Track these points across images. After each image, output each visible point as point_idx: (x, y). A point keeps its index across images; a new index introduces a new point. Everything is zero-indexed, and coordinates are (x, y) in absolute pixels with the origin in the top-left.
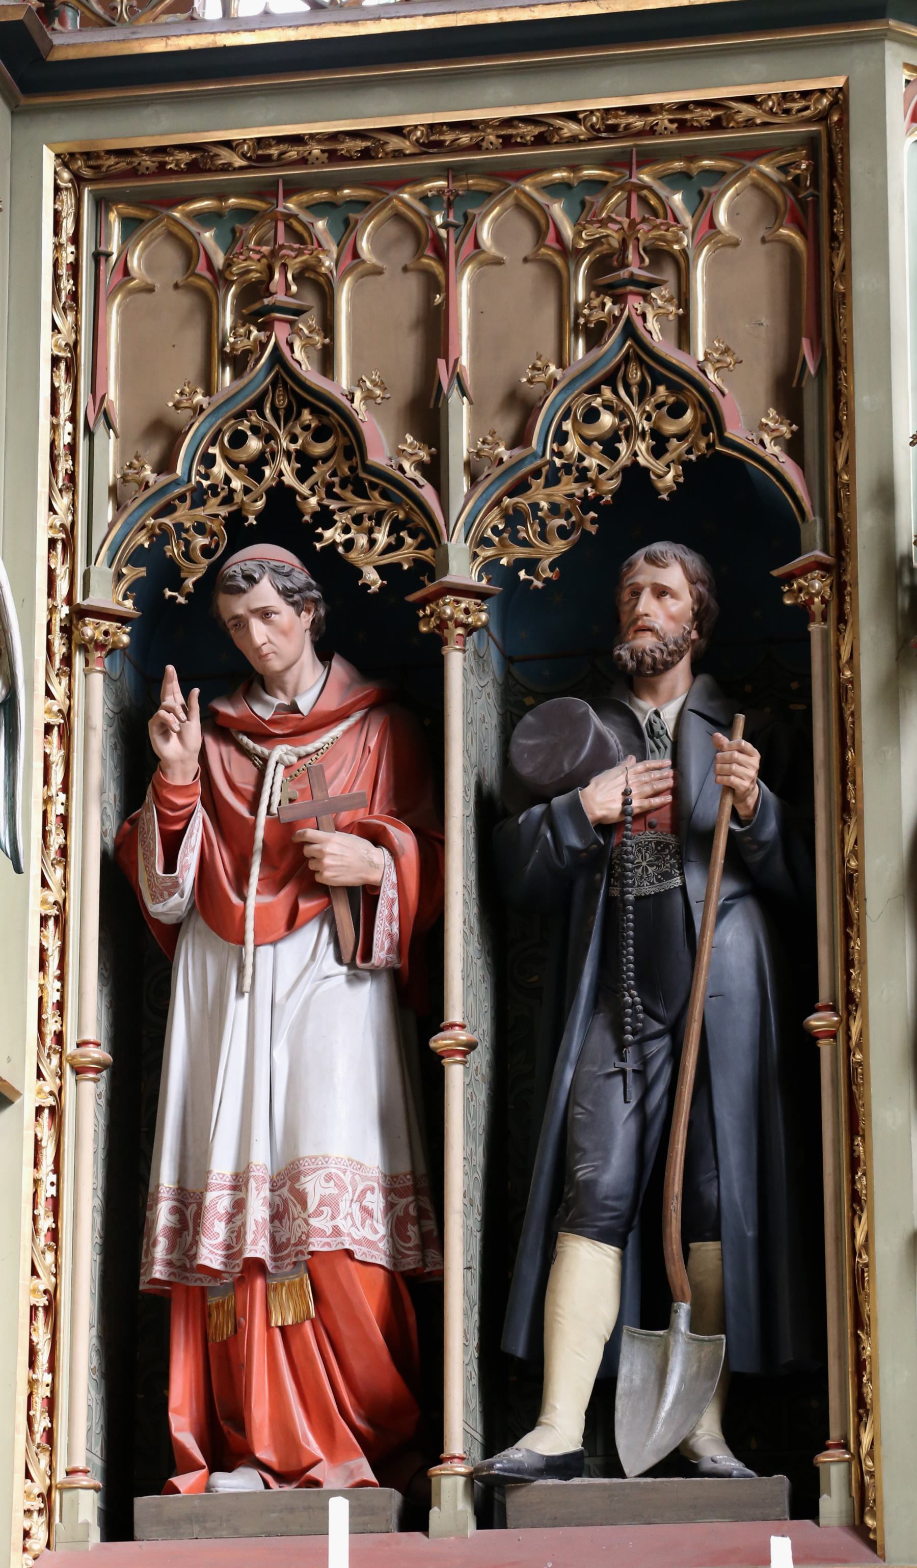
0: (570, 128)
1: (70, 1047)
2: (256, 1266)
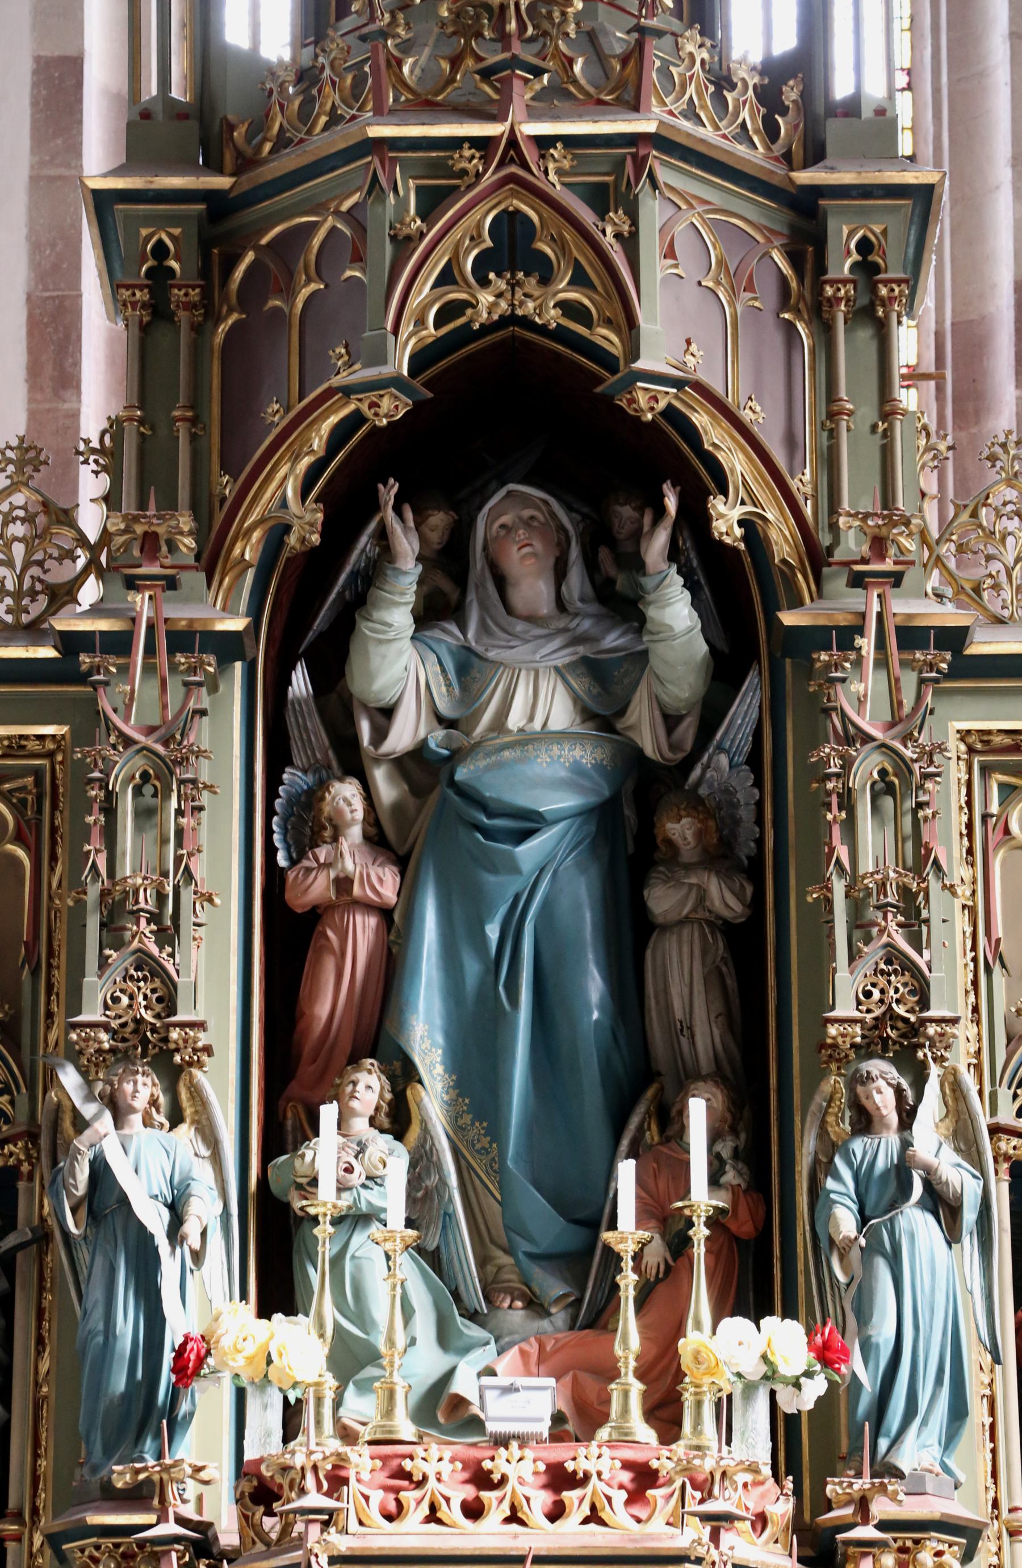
1: (1005, 1514)
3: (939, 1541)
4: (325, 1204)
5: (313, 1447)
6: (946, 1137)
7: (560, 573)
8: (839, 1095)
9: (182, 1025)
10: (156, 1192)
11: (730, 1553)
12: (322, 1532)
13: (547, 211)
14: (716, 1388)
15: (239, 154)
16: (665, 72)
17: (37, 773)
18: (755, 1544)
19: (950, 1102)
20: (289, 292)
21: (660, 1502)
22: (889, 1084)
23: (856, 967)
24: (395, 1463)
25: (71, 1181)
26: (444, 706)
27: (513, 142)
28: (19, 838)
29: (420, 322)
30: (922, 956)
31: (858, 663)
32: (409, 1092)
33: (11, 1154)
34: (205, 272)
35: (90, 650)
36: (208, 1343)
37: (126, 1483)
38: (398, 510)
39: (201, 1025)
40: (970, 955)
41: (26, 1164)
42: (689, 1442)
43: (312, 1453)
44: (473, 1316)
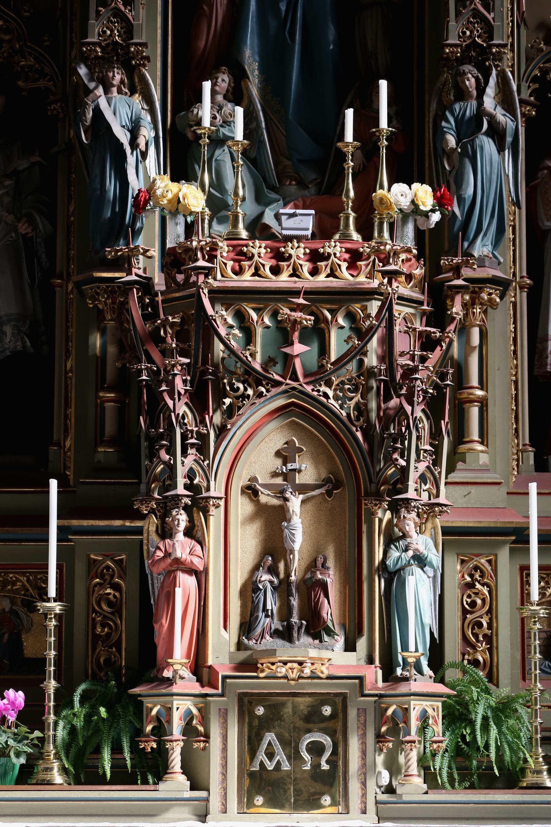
3: (491, 288)
4: (205, 128)
5: (201, 238)
6: (499, 103)
8: (448, 83)
9: (136, 44)
10: (124, 124)
11: (397, 289)
12: (205, 279)
14: (389, 216)
18: (407, 288)
19: (501, 86)
21: (363, 267)
22: (473, 76)
23: (458, 20)
24: (239, 248)
25: (84, 118)
30: (490, 14)
32: (242, 83)
33: (55, 109)
36: (150, 194)
37: (112, 256)
40: (510, 19)
41: (61, 114)
42: (377, 241)
43: (201, 241)
44: (273, 189)
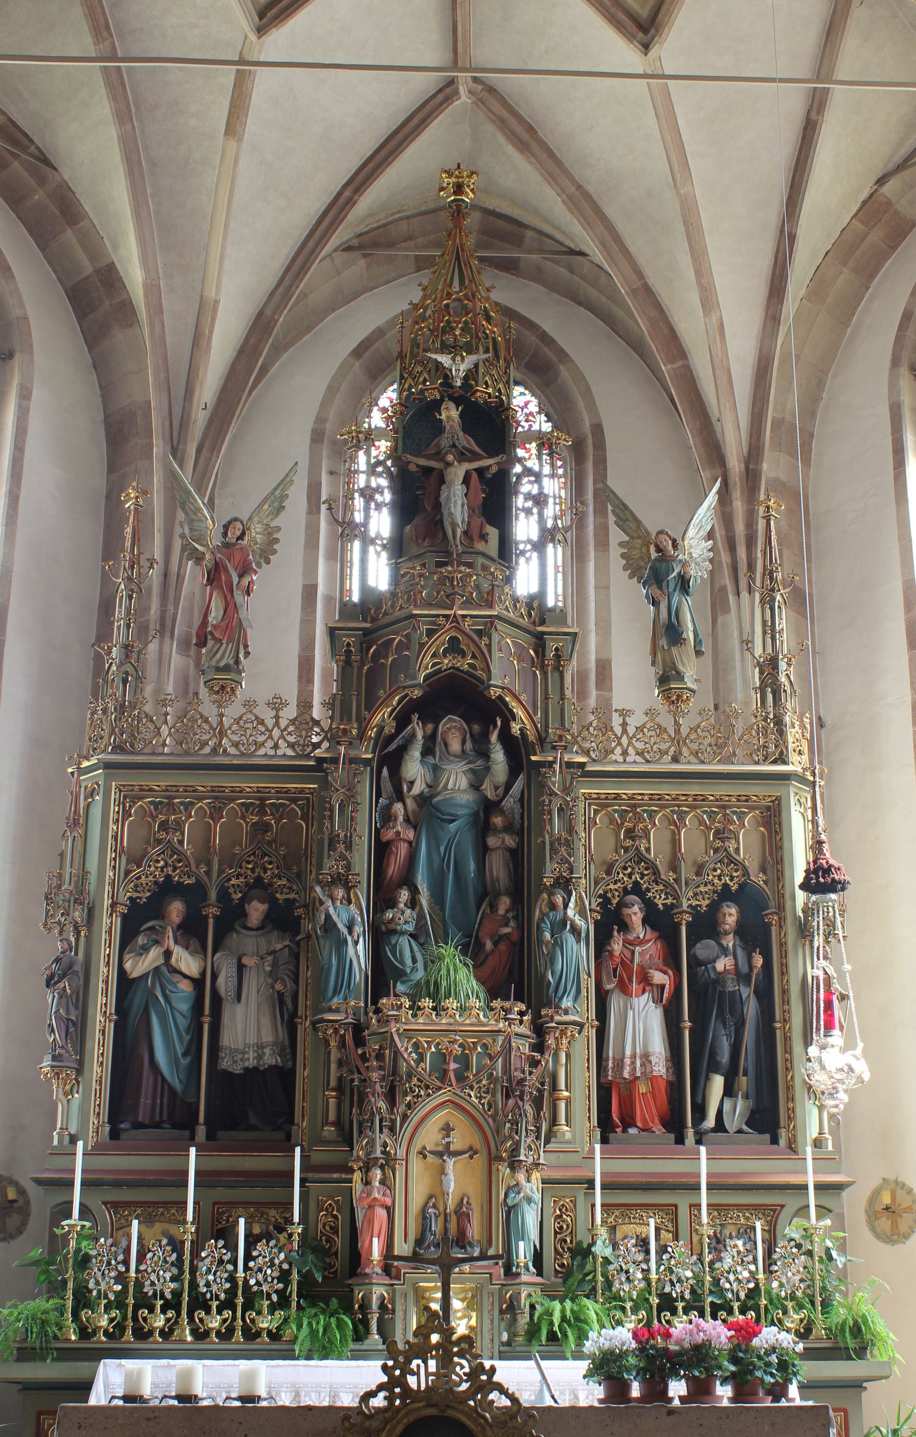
0: (711, 798)
2: (637, 1078)
7: (464, 742)
9: (353, 875)
13: (465, 637)
15: (372, 617)
16: (500, 598)
17: (308, 799)
20: (387, 659)
26: (428, 781)
27: (455, 616)
28: (302, 818)
29: (427, 668)
31: (554, 772)
34: (361, 651)
35: (326, 763)
38: (418, 723)
39: (358, 875)
